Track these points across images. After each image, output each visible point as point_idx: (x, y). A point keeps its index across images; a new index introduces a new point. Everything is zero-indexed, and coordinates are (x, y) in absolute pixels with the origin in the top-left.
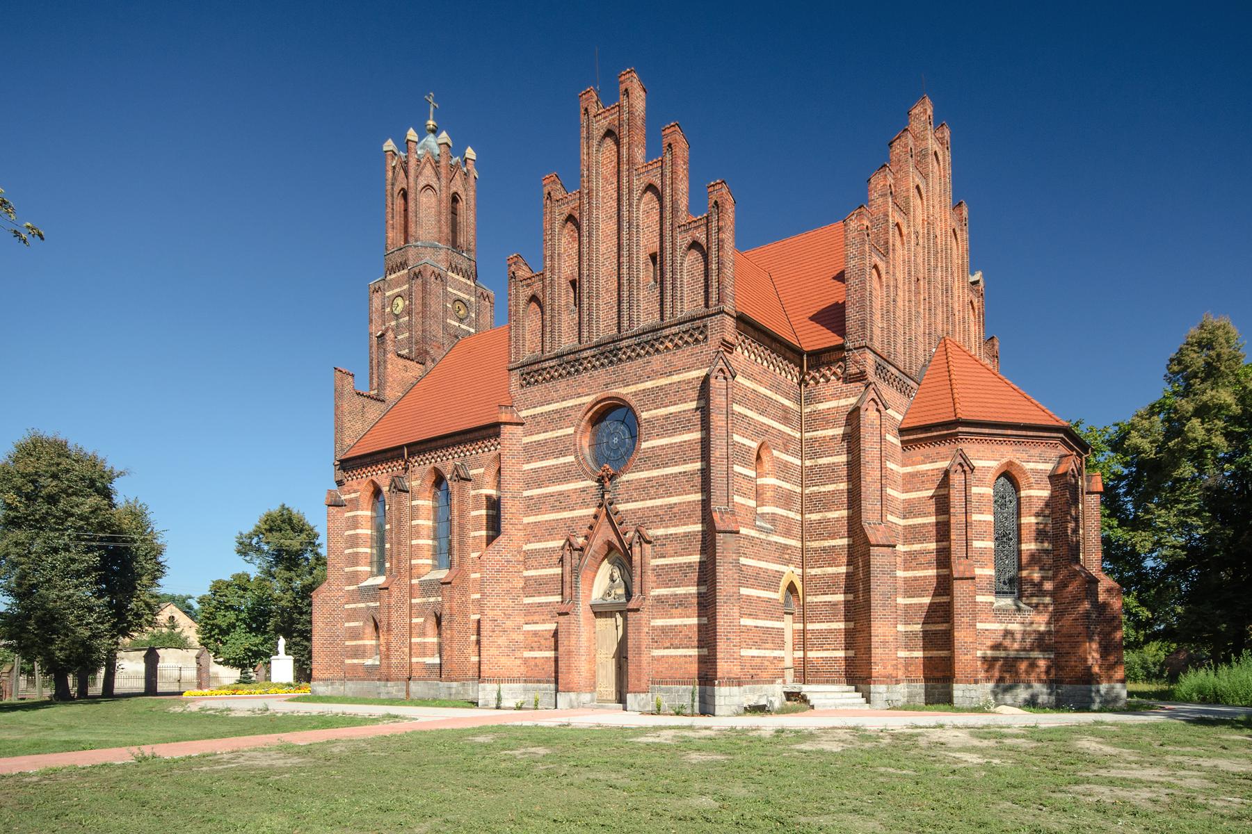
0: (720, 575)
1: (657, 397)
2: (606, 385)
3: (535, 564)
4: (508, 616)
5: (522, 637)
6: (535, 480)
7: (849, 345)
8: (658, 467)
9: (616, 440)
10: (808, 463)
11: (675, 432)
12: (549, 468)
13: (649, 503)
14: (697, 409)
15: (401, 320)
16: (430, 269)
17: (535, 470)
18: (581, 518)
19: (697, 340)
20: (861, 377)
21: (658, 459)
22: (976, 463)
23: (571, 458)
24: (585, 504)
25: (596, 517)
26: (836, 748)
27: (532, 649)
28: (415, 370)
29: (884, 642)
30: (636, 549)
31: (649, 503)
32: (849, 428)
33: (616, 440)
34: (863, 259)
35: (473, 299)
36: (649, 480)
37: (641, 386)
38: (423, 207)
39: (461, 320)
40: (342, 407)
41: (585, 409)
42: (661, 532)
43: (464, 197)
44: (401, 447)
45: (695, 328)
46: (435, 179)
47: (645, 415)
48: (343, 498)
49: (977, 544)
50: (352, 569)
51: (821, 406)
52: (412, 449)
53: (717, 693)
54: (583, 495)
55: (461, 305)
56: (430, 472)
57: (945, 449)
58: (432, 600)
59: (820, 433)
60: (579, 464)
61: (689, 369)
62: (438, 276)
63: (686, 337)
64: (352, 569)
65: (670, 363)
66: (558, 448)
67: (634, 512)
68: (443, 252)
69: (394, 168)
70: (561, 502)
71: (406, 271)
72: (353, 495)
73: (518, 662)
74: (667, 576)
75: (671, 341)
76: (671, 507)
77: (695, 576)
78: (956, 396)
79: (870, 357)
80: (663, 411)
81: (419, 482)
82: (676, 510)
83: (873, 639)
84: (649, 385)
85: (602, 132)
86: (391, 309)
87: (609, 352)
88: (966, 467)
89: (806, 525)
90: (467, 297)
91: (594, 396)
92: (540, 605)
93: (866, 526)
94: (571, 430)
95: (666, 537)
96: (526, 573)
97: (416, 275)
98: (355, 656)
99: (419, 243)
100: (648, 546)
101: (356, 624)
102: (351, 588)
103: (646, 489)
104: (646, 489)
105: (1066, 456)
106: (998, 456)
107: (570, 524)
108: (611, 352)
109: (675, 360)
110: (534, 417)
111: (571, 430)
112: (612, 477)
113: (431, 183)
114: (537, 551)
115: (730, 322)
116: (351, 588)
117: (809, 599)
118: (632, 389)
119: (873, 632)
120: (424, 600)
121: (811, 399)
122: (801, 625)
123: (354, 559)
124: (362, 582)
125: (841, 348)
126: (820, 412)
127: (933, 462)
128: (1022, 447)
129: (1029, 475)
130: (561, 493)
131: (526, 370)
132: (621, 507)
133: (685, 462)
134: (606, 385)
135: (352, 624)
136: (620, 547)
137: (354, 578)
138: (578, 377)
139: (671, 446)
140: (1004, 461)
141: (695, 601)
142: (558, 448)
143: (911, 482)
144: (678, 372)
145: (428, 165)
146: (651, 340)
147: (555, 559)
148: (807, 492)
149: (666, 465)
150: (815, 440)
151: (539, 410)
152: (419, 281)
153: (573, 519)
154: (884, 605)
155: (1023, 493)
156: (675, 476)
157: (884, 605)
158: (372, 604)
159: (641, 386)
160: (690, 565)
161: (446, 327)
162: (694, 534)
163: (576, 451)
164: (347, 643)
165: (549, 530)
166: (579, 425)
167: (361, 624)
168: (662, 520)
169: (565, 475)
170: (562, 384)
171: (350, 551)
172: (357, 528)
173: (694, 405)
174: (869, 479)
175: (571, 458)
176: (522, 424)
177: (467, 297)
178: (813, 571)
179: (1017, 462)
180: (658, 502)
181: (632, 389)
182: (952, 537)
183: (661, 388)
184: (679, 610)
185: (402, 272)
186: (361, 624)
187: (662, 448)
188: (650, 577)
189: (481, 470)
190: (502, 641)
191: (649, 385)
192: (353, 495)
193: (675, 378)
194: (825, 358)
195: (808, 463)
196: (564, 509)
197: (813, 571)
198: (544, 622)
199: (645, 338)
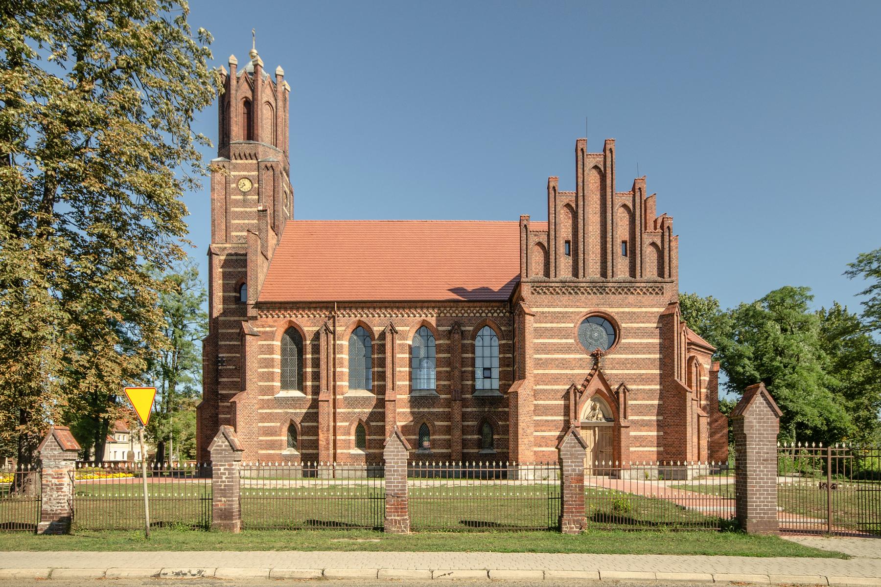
1: (632, 317)
2: (598, 305)
3: (543, 397)
6: (544, 349)
8: (632, 353)
9: (596, 334)
11: (643, 337)
12: (554, 344)
14: (657, 328)
19: (657, 293)
26: (66, 515)
27: (540, 446)
30: (621, 395)
33: (596, 334)
40: (257, 261)
44: (334, 302)
47: (623, 325)
48: (255, 329)
52: (341, 305)
56: (354, 322)
58: (357, 410)
61: (652, 307)
63: (638, 290)
65: (640, 302)
67: (616, 375)
70: (564, 364)
73: (532, 453)
74: (640, 410)
76: (641, 375)
77: (655, 411)
81: (344, 328)
82: (644, 377)
84: (627, 310)
86: (237, 185)
87: (599, 288)
91: (589, 309)
92: (547, 421)
96: (536, 402)
98: (272, 448)
103: (623, 364)
104: (623, 364)
108: (601, 287)
110: (543, 313)
111: (572, 325)
113: (270, 101)
118: (616, 310)
120: (350, 410)
123: (270, 377)
124: (277, 394)
130: (563, 359)
131: (536, 284)
133: (650, 353)
134: (598, 305)
136: (605, 391)
137: (270, 390)
139: (641, 344)
141: (655, 423)
144: (645, 307)
145: (268, 87)
146: (626, 288)
147: (560, 395)
153: (572, 375)
156: (643, 359)
160: (652, 405)
162: (655, 390)
164: (261, 438)
166: (577, 323)
167: (279, 424)
168: (635, 381)
170: (565, 298)
172: (273, 354)
173: (655, 325)
176: (534, 316)
181: (616, 310)
183: (634, 313)
184: (646, 428)
189: (408, 328)
191: (627, 310)
193: (644, 310)
198: (550, 430)
199: (624, 285)
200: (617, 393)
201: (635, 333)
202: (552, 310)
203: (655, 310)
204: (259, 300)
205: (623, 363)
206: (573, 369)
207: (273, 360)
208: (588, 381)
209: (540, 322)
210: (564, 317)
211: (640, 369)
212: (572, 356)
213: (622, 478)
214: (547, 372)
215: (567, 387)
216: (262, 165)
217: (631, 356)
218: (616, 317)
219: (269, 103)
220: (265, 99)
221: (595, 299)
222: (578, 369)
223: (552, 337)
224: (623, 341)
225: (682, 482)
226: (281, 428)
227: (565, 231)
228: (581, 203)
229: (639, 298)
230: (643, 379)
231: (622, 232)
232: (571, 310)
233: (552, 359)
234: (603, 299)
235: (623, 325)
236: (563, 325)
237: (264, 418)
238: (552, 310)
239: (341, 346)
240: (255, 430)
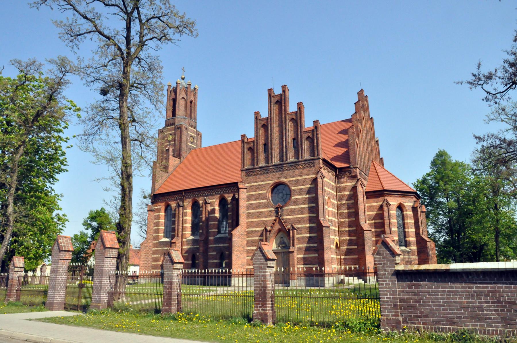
0: (324, 241)
1: (298, 183)
2: (279, 178)
4: (241, 254)
5: (246, 261)
7: (352, 167)
8: (298, 205)
10: (339, 203)
12: (257, 204)
13: (295, 216)
15: (171, 143)
16: (184, 126)
17: (251, 204)
18: (269, 220)
19: (311, 166)
20: (356, 176)
21: (297, 202)
22: (391, 203)
23: (265, 201)
24: (271, 216)
25: (275, 220)
28: (177, 160)
29: (370, 262)
30: (291, 232)
31: (295, 216)
32: (352, 193)
34: (354, 141)
35: (195, 136)
36: (295, 209)
37: (291, 179)
38: (181, 105)
39: (192, 143)
41: (270, 185)
42: (300, 226)
43: (194, 101)
45: (311, 163)
46: (185, 96)
47: (293, 188)
48: (154, 208)
49: (393, 229)
50: (156, 235)
51: (343, 185)
53: (325, 279)
54: (270, 213)
55: (192, 138)
57: (381, 199)
59: (342, 193)
60: (268, 203)
61: (308, 175)
62: (186, 128)
64: (156, 235)
65: (302, 173)
66: (261, 197)
67: (289, 219)
68: (187, 120)
69: (171, 91)
70: (261, 215)
71: (174, 126)
72: (158, 207)
75: (302, 166)
78: (382, 181)
79: (358, 170)
80: (299, 187)
81: (187, 203)
82: (305, 219)
83: (367, 261)
84: (294, 179)
85: (275, 101)
87: (279, 167)
88: (388, 205)
89: (339, 223)
90: (194, 135)
93: (361, 224)
94: (265, 192)
95: (302, 227)
97: (178, 128)
99: (179, 117)
100: (295, 231)
101: (157, 256)
102: (156, 242)
103: (294, 212)
104: (294, 212)
105: (416, 201)
106: (396, 201)
107: (265, 223)
109: (303, 171)
110: (251, 186)
111: (265, 192)
112: (281, 208)
114: (252, 231)
115: (321, 161)
116: (156, 242)
117: (341, 248)
118: (288, 180)
119: (367, 259)
121: (339, 183)
122: (339, 257)
124: (160, 239)
125: (349, 167)
126: (342, 187)
127: (376, 203)
128: (403, 198)
129: (406, 207)
130: (261, 212)
131: (248, 171)
132: (285, 217)
134: (279, 178)
135: (155, 256)
138: (268, 175)
140: (399, 202)
142: (261, 197)
143: (370, 208)
144: (304, 175)
146: (294, 165)
147: (259, 234)
148: (339, 212)
149: (301, 204)
150: (341, 195)
151: (253, 184)
152: (179, 130)
153: (266, 221)
154: (369, 250)
155: (405, 213)
157: (369, 250)
158: (165, 248)
159: (291, 179)
161: (187, 145)
163: (267, 198)
165: (257, 224)
166: (268, 190)
167: (160, 256)
168: (300, 222)
169: (263, 206)
170: (262, 177)
171: (156, 228)
174: (361, 209)
175: (265, 201)
176: (246, 189)
177: (194, 135)
178: (343, 238)
179: (402, 203)
180: (299, 216)
181: (288, 180)
182: (386, 227)
183: (298, 180)
185: (172, 127)
186: (160, 256)
187: (299, 199)
188: (296, 241)
189: (214, 200)
190: (240, 262)
191: (294, 179)
192: (158, 207)
193: (304, 177)
194: (343, 170)
195: (339, 203)
196: (263, 217)
197: (343, 238)
200: (289, 230)
201: (299, 192)
202: (256, 184)
203: (310, 176)
204: (156, 193)
205: (293, 212)
206: (266, 217)
207: (159, 222)
208: (274, 224)
209: (250, 192)
210: (261, 187)
211: (303, 214)
212: (266, 210)
213: (291, 285)
214: (253, 220)
215: (263, 228)
216: (177, 127)
217: (297, 207)
218: (288, 184)
219: (183, 98)
220: (181, 97)
221: (277, 175)
222: (269, 217)
223: (255, 200)
224: (293, 198)
225: (322, 288)
226: (160, 257)
227: (262, 141)
228: (269, 122)
229: (301, 171)
230: (300, 221)
231: (290, 135)
232: (265, 183)
233: (256, 213)
234: (281, 174)
235: (293, 188)
236: (261, 192)
237: (155, 253)
238: (256, 184)
239: (186, 213)
240: (150, 259)
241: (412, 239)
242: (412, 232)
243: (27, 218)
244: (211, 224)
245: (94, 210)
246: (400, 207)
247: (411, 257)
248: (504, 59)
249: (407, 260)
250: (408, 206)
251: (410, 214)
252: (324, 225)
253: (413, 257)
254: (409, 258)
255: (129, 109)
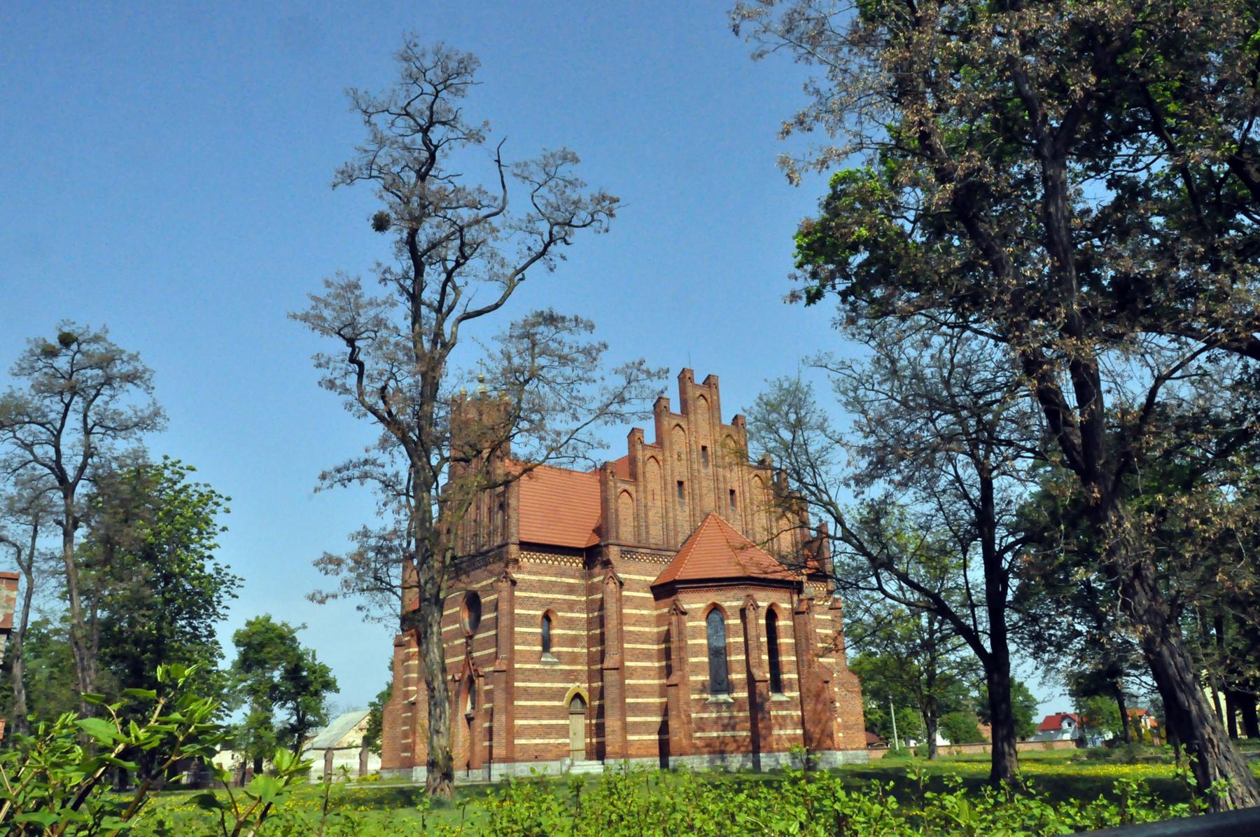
241: (738, 676)
242: (738, 661)
243: (118, 362)
244: (656, 715)
245: (276, 620)
246: (771, 615)
247: (735, 714)
248: (329, 552)
249: (726, 721)
250: (730, 607)
251: (735, 625)
252: (757, 678)
253: (741, 714)
254: (731, 718)
255: (560, 357)
